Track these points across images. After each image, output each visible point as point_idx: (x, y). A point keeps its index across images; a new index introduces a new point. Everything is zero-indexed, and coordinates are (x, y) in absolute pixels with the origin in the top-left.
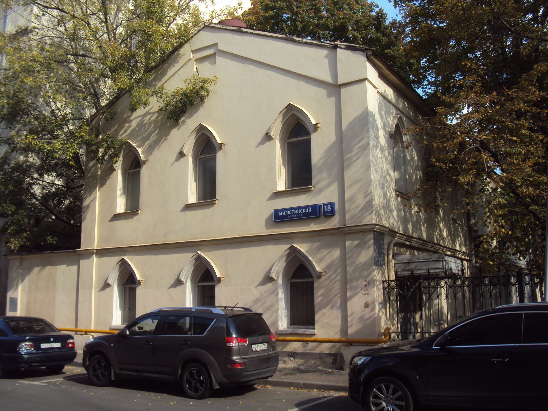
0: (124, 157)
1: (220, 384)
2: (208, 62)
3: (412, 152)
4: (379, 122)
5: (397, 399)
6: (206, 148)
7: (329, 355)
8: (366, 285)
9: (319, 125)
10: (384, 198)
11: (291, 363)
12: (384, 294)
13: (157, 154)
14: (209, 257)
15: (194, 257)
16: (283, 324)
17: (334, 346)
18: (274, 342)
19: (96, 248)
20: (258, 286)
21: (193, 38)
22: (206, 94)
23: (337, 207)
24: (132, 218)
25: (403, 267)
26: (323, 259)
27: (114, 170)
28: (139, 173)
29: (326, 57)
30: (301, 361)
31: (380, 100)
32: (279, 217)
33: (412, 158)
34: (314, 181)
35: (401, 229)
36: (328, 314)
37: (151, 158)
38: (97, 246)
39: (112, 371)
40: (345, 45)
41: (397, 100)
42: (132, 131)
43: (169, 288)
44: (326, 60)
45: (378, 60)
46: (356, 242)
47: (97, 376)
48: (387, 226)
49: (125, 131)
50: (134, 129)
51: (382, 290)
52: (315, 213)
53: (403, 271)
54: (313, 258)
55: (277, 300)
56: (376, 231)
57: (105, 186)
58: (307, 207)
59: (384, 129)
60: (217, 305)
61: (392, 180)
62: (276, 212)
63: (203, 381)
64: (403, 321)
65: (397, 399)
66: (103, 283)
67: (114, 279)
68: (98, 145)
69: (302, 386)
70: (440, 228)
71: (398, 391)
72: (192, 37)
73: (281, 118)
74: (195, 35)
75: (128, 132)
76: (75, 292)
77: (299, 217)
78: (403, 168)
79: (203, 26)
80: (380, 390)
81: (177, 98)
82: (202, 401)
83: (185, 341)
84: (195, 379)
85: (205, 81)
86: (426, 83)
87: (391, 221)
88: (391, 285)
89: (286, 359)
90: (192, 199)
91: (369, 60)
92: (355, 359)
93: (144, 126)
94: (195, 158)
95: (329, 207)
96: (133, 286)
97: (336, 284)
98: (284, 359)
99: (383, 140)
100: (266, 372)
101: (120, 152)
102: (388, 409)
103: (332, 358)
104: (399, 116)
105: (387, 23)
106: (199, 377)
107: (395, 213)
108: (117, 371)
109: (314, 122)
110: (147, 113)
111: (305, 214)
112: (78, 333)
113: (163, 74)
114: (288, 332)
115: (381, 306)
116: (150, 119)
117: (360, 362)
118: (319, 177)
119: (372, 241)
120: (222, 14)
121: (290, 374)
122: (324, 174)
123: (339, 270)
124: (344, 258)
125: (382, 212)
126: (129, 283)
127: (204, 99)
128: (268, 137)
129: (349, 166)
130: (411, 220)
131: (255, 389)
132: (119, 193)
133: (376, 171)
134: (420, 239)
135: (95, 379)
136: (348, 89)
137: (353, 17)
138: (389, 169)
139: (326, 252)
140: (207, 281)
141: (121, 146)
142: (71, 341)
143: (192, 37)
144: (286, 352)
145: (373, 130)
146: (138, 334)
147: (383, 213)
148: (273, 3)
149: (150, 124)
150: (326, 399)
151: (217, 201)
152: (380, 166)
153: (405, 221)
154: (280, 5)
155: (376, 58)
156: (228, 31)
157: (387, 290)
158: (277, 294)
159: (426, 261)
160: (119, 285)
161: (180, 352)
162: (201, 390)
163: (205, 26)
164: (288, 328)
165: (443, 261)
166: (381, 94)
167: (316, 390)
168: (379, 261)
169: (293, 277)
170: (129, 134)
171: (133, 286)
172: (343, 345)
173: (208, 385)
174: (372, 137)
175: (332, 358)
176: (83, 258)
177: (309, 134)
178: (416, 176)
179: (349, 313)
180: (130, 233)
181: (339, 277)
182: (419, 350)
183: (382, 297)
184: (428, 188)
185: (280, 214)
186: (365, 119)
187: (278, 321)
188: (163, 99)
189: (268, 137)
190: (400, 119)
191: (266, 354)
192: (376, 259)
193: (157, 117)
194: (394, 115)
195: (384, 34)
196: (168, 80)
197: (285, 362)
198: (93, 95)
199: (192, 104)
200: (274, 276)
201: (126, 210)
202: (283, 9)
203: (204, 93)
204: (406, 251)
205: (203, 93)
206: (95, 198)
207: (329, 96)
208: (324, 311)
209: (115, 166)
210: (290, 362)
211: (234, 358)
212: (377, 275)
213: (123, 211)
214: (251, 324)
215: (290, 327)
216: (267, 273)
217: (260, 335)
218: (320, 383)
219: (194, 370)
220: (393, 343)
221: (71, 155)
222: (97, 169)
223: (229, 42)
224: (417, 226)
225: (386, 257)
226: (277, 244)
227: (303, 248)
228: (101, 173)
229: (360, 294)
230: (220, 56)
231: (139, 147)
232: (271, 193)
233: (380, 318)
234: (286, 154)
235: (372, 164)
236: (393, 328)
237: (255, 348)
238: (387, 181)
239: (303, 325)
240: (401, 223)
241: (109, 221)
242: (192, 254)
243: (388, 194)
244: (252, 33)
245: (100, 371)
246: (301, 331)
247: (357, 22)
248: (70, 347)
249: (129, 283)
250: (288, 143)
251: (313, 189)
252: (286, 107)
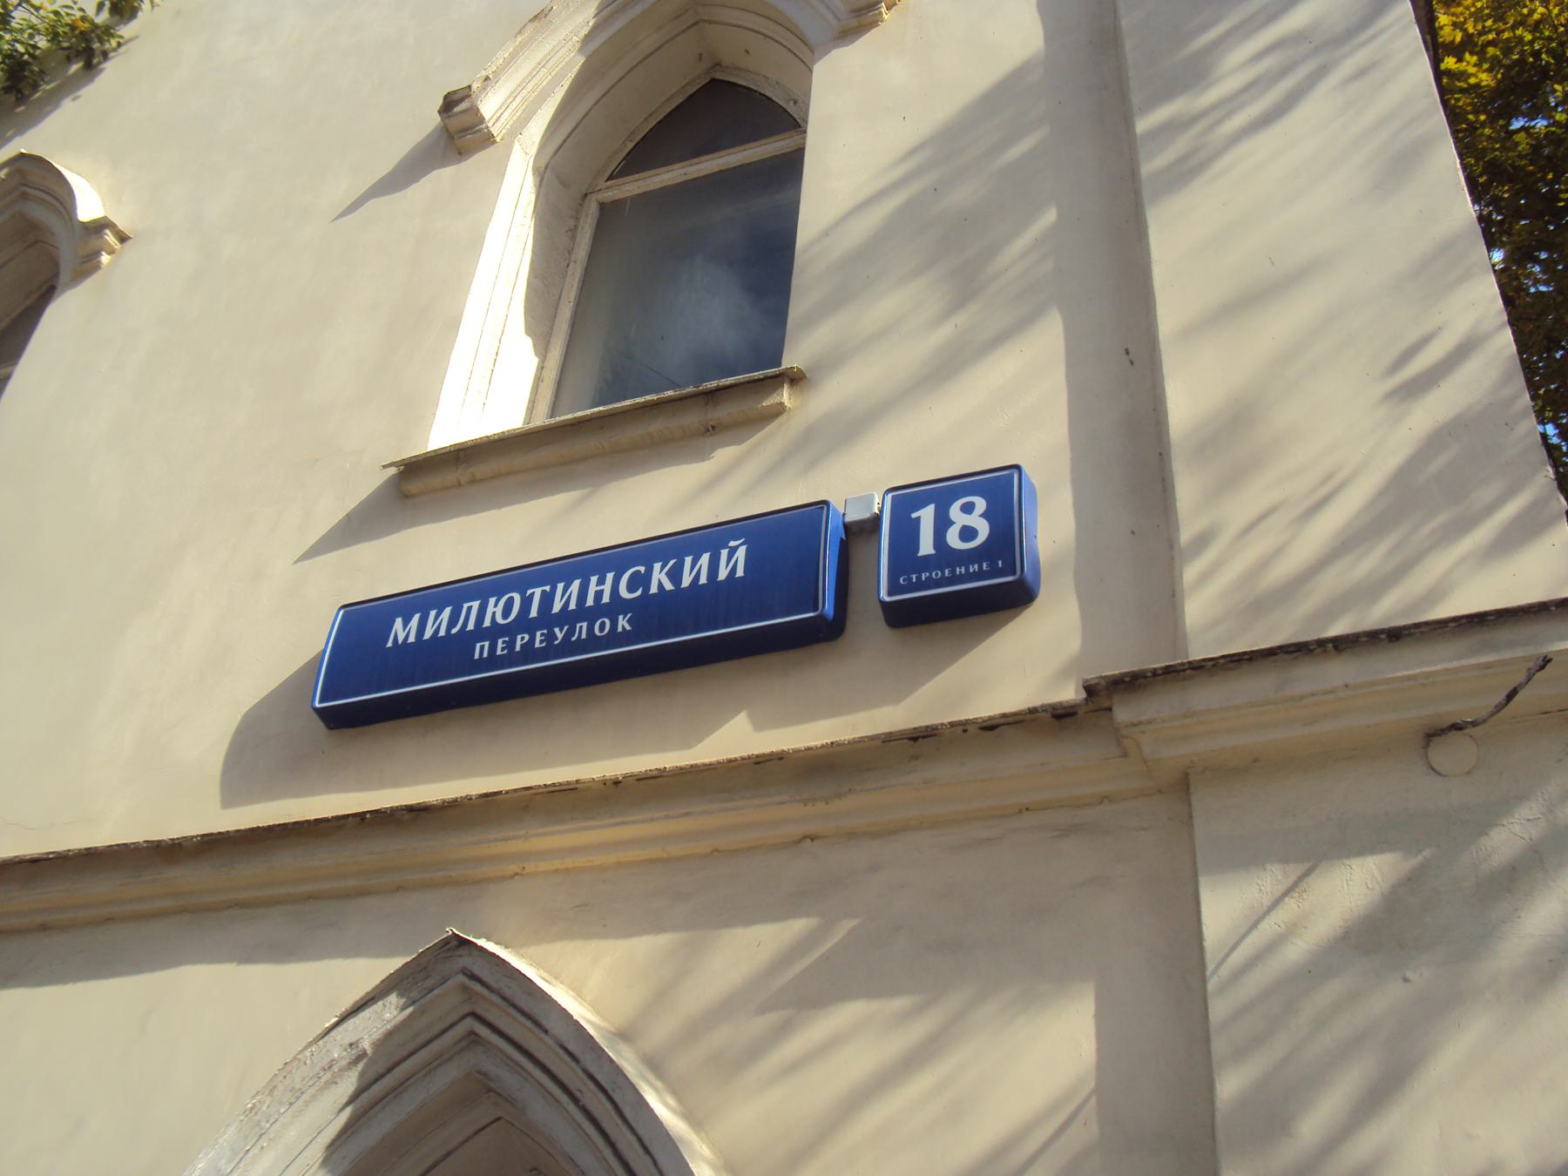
23: (1051, 529)
46: (1352, 886)
58: (710, 538)
129: (1185, 172)
185: (402, 631)
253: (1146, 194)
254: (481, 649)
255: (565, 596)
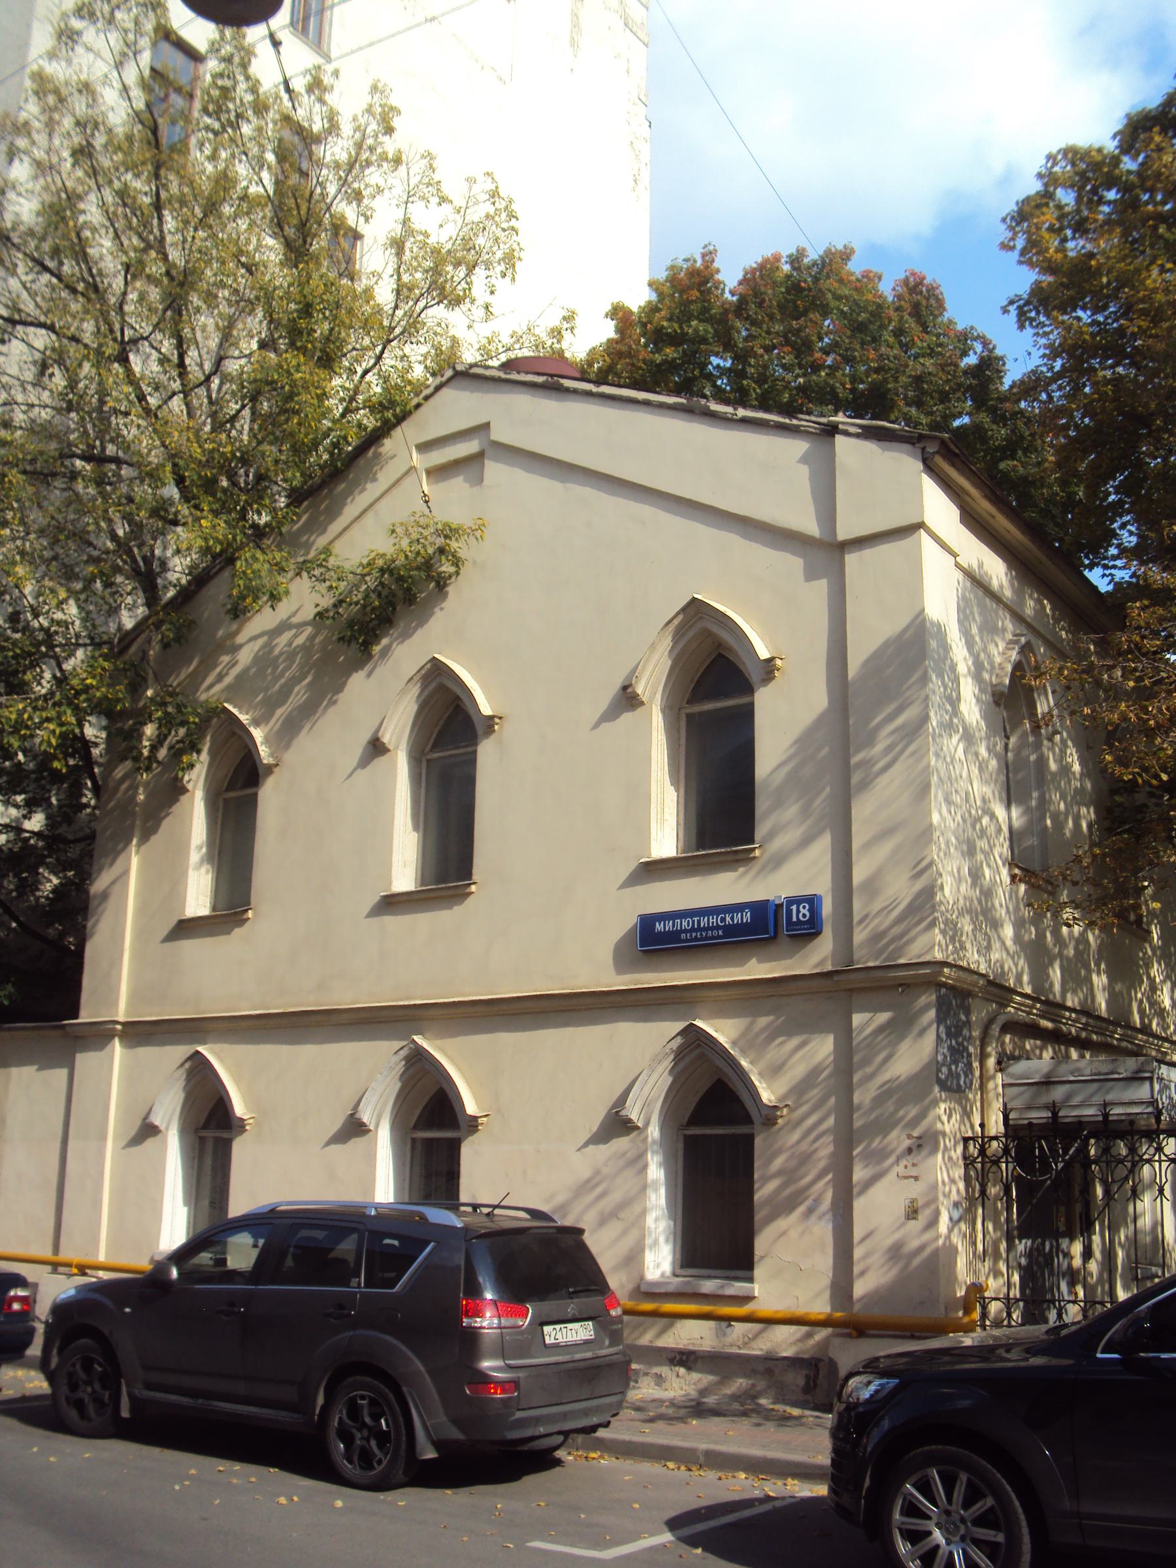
0: (213, 753)
1: (437, 1445)
2: (461, 478)
3: (1063, 752)
4: (960, 654)
5: (980, 1521)
6: (450, 730)
7: (794, 1362)
8: (910, 1150)
9: (778, 662)
10: (974, 884)
11: (680, 1385)
12: (967, 1179)
13: (306, 743)
14: (445, 1054)
15: (403, 1053)
16: (660, 1262)
17: (809, 1335)
18: (618, 1320)
19: (121, 1019)
20: (586, 1144)
21: (422, 410)
22: (452, 569)
23: (827, 908)
24: (229, 933)
25: (1028, 1093)
26: (783, 1064)
27: (184, 790)
28: (253, 800)
29: (804, 460)
30: (707, 1379)
31: (964, 589)
32: (655, 939)
33: (1065, 769)
34: (760, 832)
35: (1025, 978)
36: (794, 1234)
37: (290, 757)
38: (127, 1013)
39: (124, 1389)
40: (860, 426)
41: (1018, 593)
42: (239, 677)
43: (328, 1143)
44: (804, 471)
45: (958, 469)
46: (883, 1017)
47: (79, 1405)
48: (983, 969)
49: (220, 677)
50: (246, 671)
51: (961, 1162)
52: (764, 926)
53: (1029, 1108)
54: (751, 1063)
55: (644, 1188)
56: (945, 985)
57: (154, 838)
59: (977, 676)
60: (463, 1198)
61: (1000, 830)
62: (647, 923)
63: (387, 1433)
64: (1030, 1264)
65: (980, 1521)
66: (139, 1123)
67: (168, 1113)
68: (143, 717)
69: (702, 1459)
70: (1152, 981)
71: (984, 1496)
72: (418, 406)
73: (667, 642)
74: (426, 398)
75: (228, 680)
76: (57, 1145)
77: (713, 938)
78: (1035, 794)
79: (449, 373)
80: (925, 1488)
81: (371, 582)
82: (382, 1496)
83: (341, 1307)
84: (364, 1425)
85: (449, 532)
86: (1113, 551)
87: (995, 956)
88: (989, 1152)
89: (664, 1370)
90: (404, 880)
91: (930, 468)
92: (852, 1382)
93: (274, 662)
94: (417, 758)
95: (805, 911)
96: (225, 1135)
97: (822, 1141)
98: (657, 1370)
99: (971, 710)
100: (586, 1413)
101: (202, 737)
102: (951, 1554)
103: (805, 1372)
104: (1023, 640)
105: (1007, 382)
106: (376, 1418)
107: (1008, 931)
108: (137, 1392)
109: (763, 653)
110: (283, 627)
111: (731, 931)
112: (61, 1269)
113: (333, 513)
114: (671, 1289)
115: (956, 1215)
116: (290, 644)
117: (866, 1394)
118: (778, 821)
119: (932, 1013)
120: (517, 346)
121: (669, 1419)
122: (791, 811)
123: (832, 1100)
124: (847, 1062)
125: (966, 925)
126: (212, 1125)
127: (445, 585)
128: (628, 699)
129: (865, 785)
130: (1060, 954)
131: (558, 1462)
132: (195, 856)
133: (948, 802)
134: (1087, 1011)
135: (73, 1414)
136: (869, 554)
137: (907, 366)
138: (989, 795)
139: (795, 1041)
140: (441, 1126)
141: (205, 721)
142: (21, 1293)
143: (418, 406)
144: (665, 1349)
145: (940, 675)
146: (208, 1278)
147: (968, 928)
148: (676, 326)
149: (291, 656)
150: (767, 1507)
151: (473, 888)
152: (963, 785)
153: (1037, 955)
154: (696, 331)
155: (953, 465)
156: (522, 389)
157: (979, 1163)
158: (646, 1167)
159: (1102, 1080)
160: (183, 1132)
161: (323, 1340)
162: (380, 1462)
163: (458, 374)
164: (675, 1275)
165: (1151, 1079)
166: (969, 574)
167: (743, 1475)
168: (951, 1078)
169: (694, 1120)
170: (229, 688)
171: (225, 1135)
172: (838, 1335)
173: (403, 1446)
174: (936, 699)
175: (805, 1372)
176: (86, 1048)
177: (749, 690)
178: (1077, 825)
179: (858, 1234)
180: (222, 978)
181: (831, 1121)
182: (1070, 1362)
183: (962, 1185)
184: (1104, 855)
185: (659, 927)
186: (915, 647)
187: (642, 1251)
188: (328, 584)
189: (628, 699)
190: (1026, 649)
191: (589, 1355)
192: (944, 1070)
193: (311, 638)
194: (1009, 636)
195: (999, 418)
196: (345, 529)
197: (659, 1380)
199: (410, 599)
200: (634, 1116)
201: (214, 909)
202: (704, 340)
203: (447, 568)
204: (1042, 1049)
205: (443, 569)
206: (126, 872)
207: (811, 575)
208: (781, 1224)
209: (186, 778)
210: (676, 1383)
211: (486, 1364)
212: (946, 1119)
213: (205, 911)
214: (547, 1262)
215: (679, 1271)
216: (614, 1107)
217: (571, 1296)
218: (756, 1452)
219: (363, 1398)
220: (996, 1332)
221: (54, 741)
222: (134, 788)
223: (522, 418)
224: (1076, 976)
225: (976, 1064)
226: (646, 1019)
227: (722, 1031)
228: (147, 797)
229: (891, 1176)
230: (497, 460)
231: (257, 723)
232: (633, 866)
233: (954, 1251)
234: (683, 750)
235: (934, 779)
236: (994, 1286)
237: (554, 1334)
238: (983, 832)
239: (722, 1268)
240: (1027, 959)
242: (397, 1044)
243: (987, 872)
244: (589, 394)
245: (89, 1389)
246: (709, 1286)
247: (918, 380)
248: (17, 1313)
249: (212, 1125)
250: (689, 717)
251: (757, 853)
252: (684, 610)
253: (852, 792)
254: (683, 936)
255: (704, 922)
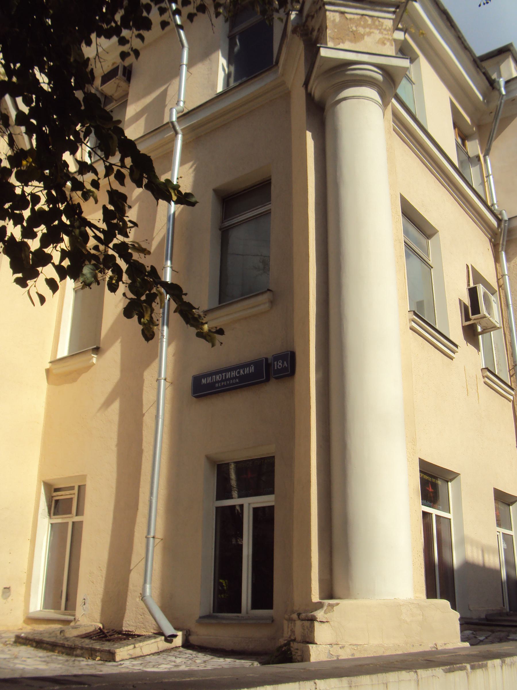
58: (247, 365)
77: (233, 384)
185: (204, 381)
198: (361, 18)
241: (460, 301)
